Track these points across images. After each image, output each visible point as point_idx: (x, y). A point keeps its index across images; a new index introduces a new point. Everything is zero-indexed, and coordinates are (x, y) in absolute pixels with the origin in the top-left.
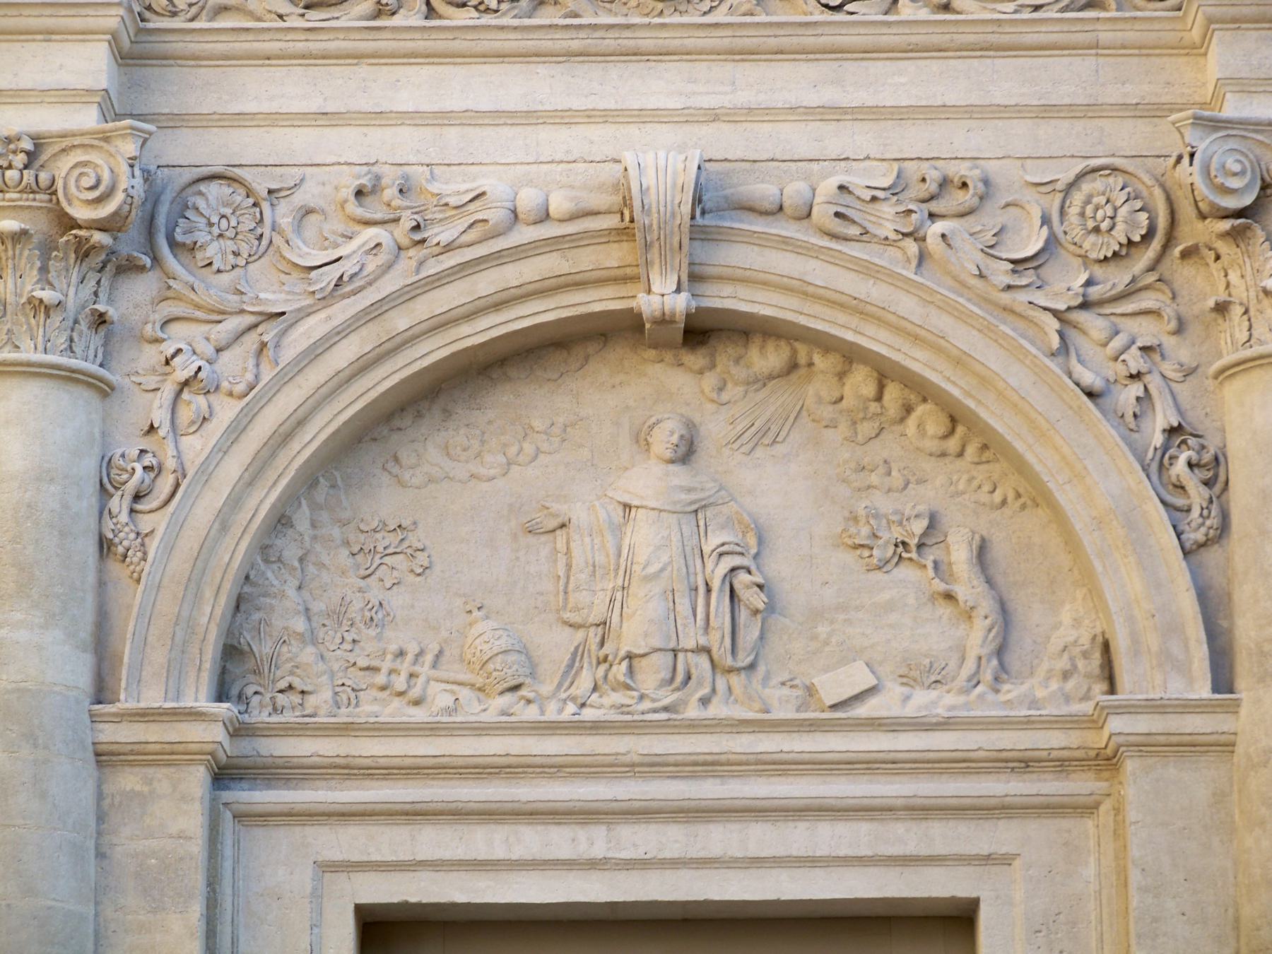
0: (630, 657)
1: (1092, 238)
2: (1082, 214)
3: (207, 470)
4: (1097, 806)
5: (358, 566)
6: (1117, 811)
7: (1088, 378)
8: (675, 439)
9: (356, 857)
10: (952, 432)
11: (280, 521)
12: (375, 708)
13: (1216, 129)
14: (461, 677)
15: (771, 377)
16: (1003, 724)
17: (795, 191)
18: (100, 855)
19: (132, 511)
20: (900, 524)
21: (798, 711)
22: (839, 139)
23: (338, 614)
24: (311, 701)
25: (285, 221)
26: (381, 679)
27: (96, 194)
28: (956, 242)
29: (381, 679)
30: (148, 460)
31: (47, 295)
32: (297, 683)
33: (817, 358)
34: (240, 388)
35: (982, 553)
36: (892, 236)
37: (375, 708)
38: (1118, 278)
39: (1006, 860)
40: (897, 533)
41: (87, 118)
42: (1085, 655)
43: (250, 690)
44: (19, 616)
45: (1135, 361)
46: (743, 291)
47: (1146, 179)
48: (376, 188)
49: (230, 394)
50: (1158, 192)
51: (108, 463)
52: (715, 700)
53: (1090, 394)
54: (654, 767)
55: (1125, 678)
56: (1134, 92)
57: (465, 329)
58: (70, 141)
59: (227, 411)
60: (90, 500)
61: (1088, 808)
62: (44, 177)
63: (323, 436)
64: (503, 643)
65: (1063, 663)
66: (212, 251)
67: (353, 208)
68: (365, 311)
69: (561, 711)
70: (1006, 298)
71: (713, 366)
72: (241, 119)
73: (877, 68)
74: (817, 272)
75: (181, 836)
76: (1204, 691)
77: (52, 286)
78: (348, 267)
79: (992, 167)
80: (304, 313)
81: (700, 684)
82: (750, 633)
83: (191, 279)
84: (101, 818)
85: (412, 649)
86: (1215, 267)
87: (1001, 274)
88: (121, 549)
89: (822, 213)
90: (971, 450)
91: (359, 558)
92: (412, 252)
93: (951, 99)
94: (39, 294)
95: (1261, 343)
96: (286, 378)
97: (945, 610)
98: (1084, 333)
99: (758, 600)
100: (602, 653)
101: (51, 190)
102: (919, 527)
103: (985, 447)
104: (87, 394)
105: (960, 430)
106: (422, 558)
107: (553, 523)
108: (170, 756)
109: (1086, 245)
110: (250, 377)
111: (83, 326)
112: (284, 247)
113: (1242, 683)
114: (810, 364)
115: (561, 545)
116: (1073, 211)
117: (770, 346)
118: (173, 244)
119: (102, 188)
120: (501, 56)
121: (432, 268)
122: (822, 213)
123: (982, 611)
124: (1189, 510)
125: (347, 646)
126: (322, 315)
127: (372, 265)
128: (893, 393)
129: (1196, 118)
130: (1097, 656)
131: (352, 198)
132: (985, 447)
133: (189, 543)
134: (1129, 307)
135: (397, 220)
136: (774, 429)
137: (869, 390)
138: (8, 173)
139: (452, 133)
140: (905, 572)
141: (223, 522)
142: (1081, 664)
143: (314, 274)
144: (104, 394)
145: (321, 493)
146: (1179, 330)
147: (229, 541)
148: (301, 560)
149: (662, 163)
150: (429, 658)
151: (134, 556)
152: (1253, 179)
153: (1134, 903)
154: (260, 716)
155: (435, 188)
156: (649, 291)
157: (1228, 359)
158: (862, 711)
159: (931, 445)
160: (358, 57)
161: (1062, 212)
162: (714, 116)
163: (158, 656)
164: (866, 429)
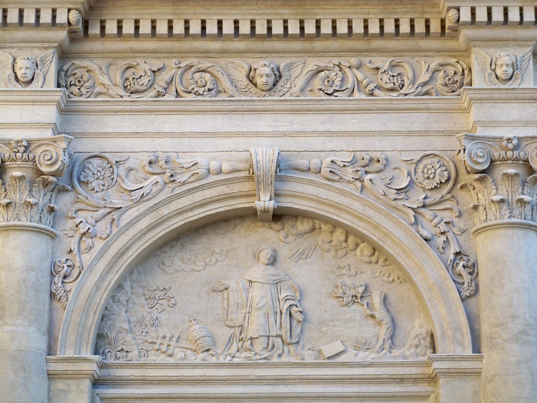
0: (251, 339)
1: (427, 181)
2: (423, 172)
3: (91, 267)
4: (428, 396)
7: (425, 234)
8: (269, 256)
11: (119, 286)
12: (154, 358)
13: (474, 140)
14: (187, 346)
15: (305, 233)
17: (315, 163)
19: (63, 282)
20: (354, 289)
24: (130, 355)
26: (157, 346)
27: (51, 162)
28: (375, 182)
29: (157, 346)
30: (69, 263)
31: (32, 200)
32: (125, 348)
34: (104, 236)
35: (385, 300)
36: (351, 180)
37: (154, 358)
38: (436, 196)
40: (353, 292)
42: (424, 339)
45: (443, 227)
46: (295, 200)
49: (101, 238)
50: (451, 164)
52: (284, 355)
56: (442, 126)
57: (190, 214)
58: (41, 142)
59: (99, 244)
62: (31, 156)
64: (203, 333)
65: (416, 342)
67: (148, 168)
69: (225, 359)
70: (394, 203)
71: (283, 229)
73: (346, 117)
74: (323, 193)
76: (469, 352)
78: (146, 190)
79: (389, 154)
80: (129, 208)
81: (278, 349)
82: (297, 330)
83: (86, 195)
85: (169, 335)
86: (473, 192)
87: (392, 194)
89: (325, 171)
90: (381, 261)
92: (170, 185)
93: (373, 129)
94: (28, 200)
95: (491, 220)
96: (121, 232)
97: (371, 321)
99: (300, 317)
101: (34, 160)
102: (361, 290)
105: (377, 253)
106: (173, 301)
107: (223, 288)
108: (76, 376)
109: (424, 184)
110: (108, 232)
111: (45, 212)
113: (484, 349)
114: (320, 228)
116: (420, 171)
118: (80, 182)
119: (53, 160)
120: (204, 112)
122: (325, 171)
124: (463, 284)
126: (136, 209)
128: (351, 239)
130: (429, 339)
131: (147, 164)
133: (84, 294)
135: (164, 173)
136: (306, 253)
137: (342, 238)
138: (18, 154)
140: (356, 307)
141: (97, 286)
142: (422, 342)
143: (133, 193)
144: (53, 238)
145: (135, 276)
146: (460, 216)
147: (99, 294)
148: (127, 301)
150: (175, 339)
151: (63, 300)
152: (487, 159)
154: (111, 360)
155: (179, 161)
156: (259, 200)
158: (339, 359)
161: (415, 171)
162: (284, 134)
163: (72, 337)
164: (341, 253)
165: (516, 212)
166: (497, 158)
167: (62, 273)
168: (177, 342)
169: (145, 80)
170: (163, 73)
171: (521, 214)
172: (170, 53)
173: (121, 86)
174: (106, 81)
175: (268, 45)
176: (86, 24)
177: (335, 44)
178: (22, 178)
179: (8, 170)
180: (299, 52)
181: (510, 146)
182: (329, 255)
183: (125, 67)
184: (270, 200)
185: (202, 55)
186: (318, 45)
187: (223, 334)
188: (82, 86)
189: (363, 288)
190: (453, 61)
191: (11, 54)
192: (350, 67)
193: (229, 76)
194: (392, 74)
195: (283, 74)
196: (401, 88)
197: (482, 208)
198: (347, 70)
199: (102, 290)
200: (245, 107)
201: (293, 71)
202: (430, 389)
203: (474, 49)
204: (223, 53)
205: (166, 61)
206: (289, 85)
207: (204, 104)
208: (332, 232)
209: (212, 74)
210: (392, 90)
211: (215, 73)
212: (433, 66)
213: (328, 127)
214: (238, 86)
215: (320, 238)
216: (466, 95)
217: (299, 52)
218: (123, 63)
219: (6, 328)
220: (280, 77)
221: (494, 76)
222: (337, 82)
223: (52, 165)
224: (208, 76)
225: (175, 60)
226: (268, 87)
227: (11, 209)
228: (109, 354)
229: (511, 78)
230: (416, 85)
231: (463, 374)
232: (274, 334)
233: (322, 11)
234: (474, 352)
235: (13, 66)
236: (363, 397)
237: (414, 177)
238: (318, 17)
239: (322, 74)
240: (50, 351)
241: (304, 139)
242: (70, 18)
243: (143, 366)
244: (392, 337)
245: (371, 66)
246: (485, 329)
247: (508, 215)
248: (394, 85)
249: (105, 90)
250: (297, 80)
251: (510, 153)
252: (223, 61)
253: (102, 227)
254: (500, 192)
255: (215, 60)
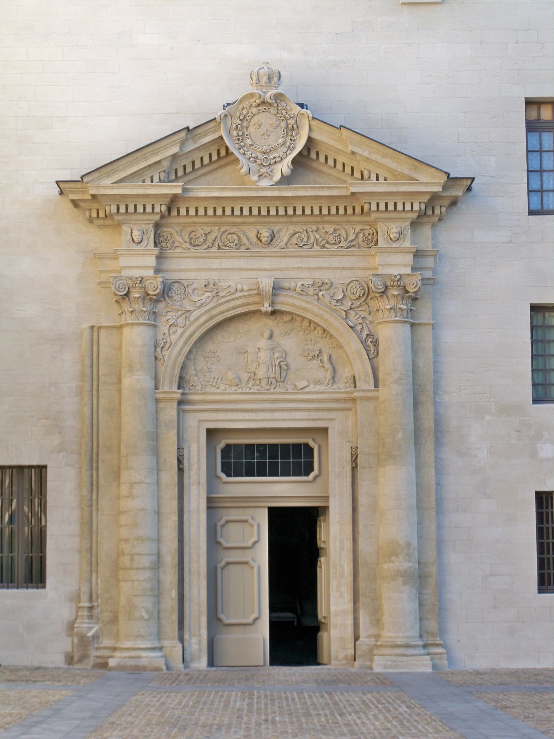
0: (260, 379)
1: (352, 295)
2: (351, 290)
3: (176, 343)
4: (352, 409)
5: (205, 360)
6: (356, 410)
7: (351, 324)
8: (269, 334)
9: (206, 419)
10: (324, 333)
11: (190, 351)
12: (209, 389)
13: (377, 276)
14: (226, 383)
15: (288, 321)
16: (334, 393)
17: (293, 285)
18: (157, 419)
19: (161, 351)
20: (314, 351)
21: (293, 390)
22: (301, 274)
23: (202, 370)
24: (197, 388)
25: (191, 291)
26: (210, 383)
27: (154, 289)
28: (325, 296)
29: (210, 383)
30: (164, 341)
31: (144, 309)
32: (194, 384)
33: (297, 318)
34: (182, 326)
35: (330, 358)
36: (312, 294)
37: (209, 389)
38: (357, 303)
39: (334, 419)
40: (313, 354)
41: (151, 273)
42: (350, 379)
43: (185, 386)
44: (140, 374)
45: (360, 320)
46: (283, 306)
47: (364, 283)
48: (209, 284)
49: (180, 327)
50: (366, 285)
51: (156, 341)
52: (277, 388)
53: (351, 327)
54: (264, 401)
55: (358, 385)
56: (361, 265)
57: (227, 314)
58: (148, 278)
59: (180, 331)
60: (153, 349)
61: (349, 409)
62: (143, 285)
63: (199, 336)
64: (235, 376)
65: (346, 380)
66: (176, 298)
67: (204, 289)
68: (207, 311)
69: (246, 390)
70: (335, 308)
71: (276, 319)
72: (181, 270)
73: (309, 260)
74: (297, 302)
75: (173, 416)
76: (372, 388)
77: (145, 307)
78: (203, 301)
79: (332, 280)
80: (195, 310)
81: (274, 384)
82: (283, 374)
83: (172, 303)
84: (157, 412)
85: (217, 377)
86: (377, 301)
88: (159, 359)
89: (298, 290)
90: (328, 337)
91: (206, 358)
92: (216, 298)
93: (324, 266)
94: (142, 309)
95: (385, 318)
96: (190, 325)
97: (322, 369)
98: (350, 314)
99: (285, 368)
100: (254, 378)
101: (145, 287)
102: (317, 352)
103: (331, 336)
104: (152, 328)
105: (326, 332)
106: (218, 359)
107: (245, 351)
108: (170, 400)
109: (351, 296)
110: (184, 324)
111: (151, 314)
112: (190, 297)
113: (380, 386)
114: (296, 319)
115: (246, 355)
116: (349, 289)
117: (288, 316)
118: (168, 296)
119: (155, 288)
120: (234, 257)
121: (220, 302)
122: (298, 290)
123: (330, 370)
124: (371, 351)
125: (203, 377)
126: (198, 311)
127: (208, 301)
128: (312, 325)
129: (372, 274)
130: (352, 379)
131: (204, 287)
132: (331, 336)
133: (173, 357)
134: (360, 309)
135: (213, 291)
136: (289, 332)
137: (307, 324)
138: (137, 285)
139: (224, 273)
140: (314, 362)
141: (179, 353)
142: (349, 380)
143: (196, 303)
144: (155, 327)
145: (198, 346)
146: (370, 313)
147: (180, 357)
148: (194, 359)
149: (266, 281)
150: (220, 379)
151: (162, 360)
152: (384, 286)
153: (358, 429)
154: (187, 391)
155: (220, 284)
156: (264, 306)
157: (379, 321)
158: (305, 390)
159: (320, 336)
160: (205, 257)
161: (346, 289)
163: (167, 380)
164: (307, 332)
165: (398, 314)
166: (389, 285)
167: (161, 346)
168: (221, 381)
169: (201, 240)
170: (211, 235)
171: (401, 315)
172: (215, 223)
173: (189, 243)
174: (181, 240)
175: (267, 219)
176: (169, 210)
177: (304, 219)
178: (138, 298)
179: (131, 292)
180: (284, 223)
181: (396, 279)
182: (301, 333)
183: (190, 231)
184: (269, 306)
185: (232, 224)
186: (295, 219)
187: (245, 376)
188: (167, 242)
189: (319, 352)
190: (368, 227)
191: (130, 227)
192: (312, 231)
193: (246, 236)
194: (335, 235)
195: (276, 236)
196: (340, 243)
197: (381, 311)
198: (310, 233)
199: (182, 355)
200: (255, 255)
201: (281, 233)
202: (352, 405)
203: (378, 223)
204: (243, 223)
205: (213, 228)
206: (279, 241)
207: (234, 253)
208: (302, 321)
209: (238, 236)
210: (335, 244)
211: (239, 235)
212: (357, 231)
213: (300, 265)
214: (252, 241)
215: (296, 324)
216: (373, 250)
217: (284, 223)
218: (189, 229)
219: (134, 377)
220: (274, 236)
221: (389, 238)
222: (305, 239)
223: (155, 290)
224: (235, 237)
225: (217, 228)
226: (268, 243)
227: (134, 313)
228: (186, 388)
229: (398, 239)
230: (348, 241)
231: (369, 398)
232: (272, 376)
233: (297, 202)
234: (375, 387)
235: (131, 234)
236: (318, 409)
237: (346, 293)
238: (294, 206)
239: (297, 235)
240: (156, 388)
241: (287, 272)
242: (162, 209)
243: (204, 394)
244: (333, 378)
245: (323, 231)
246: (381, 376)
247: (394, 316)
248: (336, 241)
249: (180, 245)
250: (283, 238)
251: (395, 283)
252: (243, 228)
253: (181, 321)
254: (390, 303)
255: (239, 227)
